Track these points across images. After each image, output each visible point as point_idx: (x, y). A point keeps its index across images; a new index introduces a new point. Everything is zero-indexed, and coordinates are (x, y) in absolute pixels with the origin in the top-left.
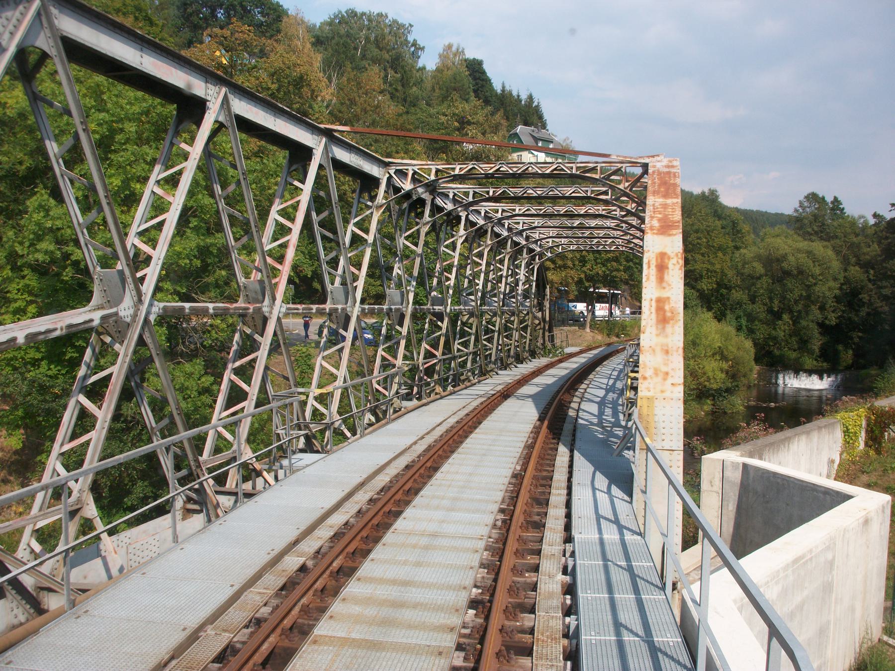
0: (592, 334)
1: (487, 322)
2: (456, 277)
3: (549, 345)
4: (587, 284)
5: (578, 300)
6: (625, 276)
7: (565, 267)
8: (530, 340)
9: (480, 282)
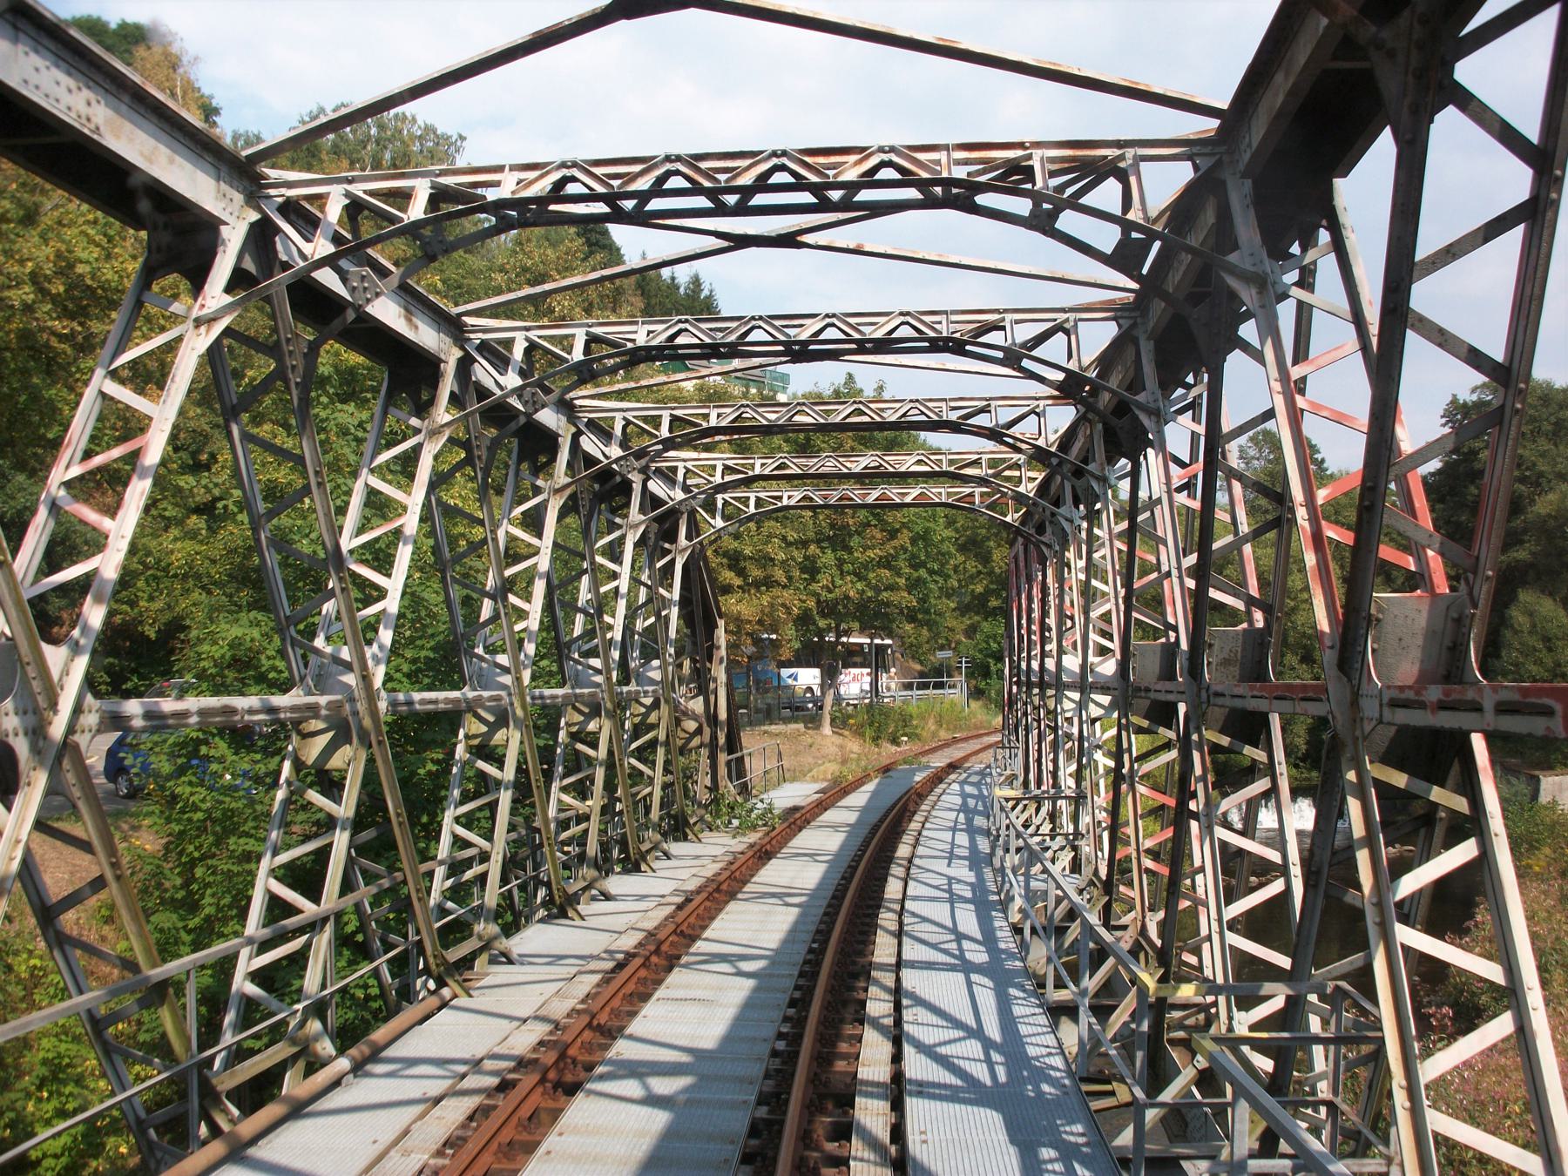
0: (838, 740)
1: (470, 749)
2: (549, 607)
3: (729, 789)
4: (822, 623)
5: (801, 660)
6: (907, 599)
7: (769, 583)
8: (665, 786)
9: (617, 621)
